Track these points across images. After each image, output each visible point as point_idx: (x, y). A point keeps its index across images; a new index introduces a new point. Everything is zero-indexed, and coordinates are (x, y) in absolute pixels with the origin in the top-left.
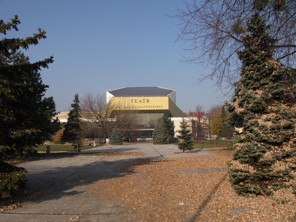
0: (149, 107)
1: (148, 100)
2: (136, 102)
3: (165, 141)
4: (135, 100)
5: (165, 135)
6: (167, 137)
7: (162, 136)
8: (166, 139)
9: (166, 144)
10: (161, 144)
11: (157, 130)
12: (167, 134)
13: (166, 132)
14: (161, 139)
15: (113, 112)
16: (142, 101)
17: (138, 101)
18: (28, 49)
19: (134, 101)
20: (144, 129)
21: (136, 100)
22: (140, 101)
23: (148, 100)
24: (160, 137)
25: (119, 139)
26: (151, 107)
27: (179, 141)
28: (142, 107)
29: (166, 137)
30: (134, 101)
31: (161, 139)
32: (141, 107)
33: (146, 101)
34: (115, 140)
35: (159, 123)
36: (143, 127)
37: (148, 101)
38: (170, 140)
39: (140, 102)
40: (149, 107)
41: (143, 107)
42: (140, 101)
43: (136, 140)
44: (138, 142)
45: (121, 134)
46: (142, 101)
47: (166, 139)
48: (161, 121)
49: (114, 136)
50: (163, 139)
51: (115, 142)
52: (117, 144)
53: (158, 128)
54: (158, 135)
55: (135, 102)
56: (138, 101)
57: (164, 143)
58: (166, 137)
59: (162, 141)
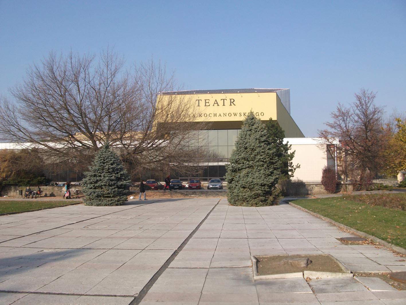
0: (235, 115)
1: (232, 101)
2: (207, 104)
3: (269, 193)
4: (205, 100)
5: (268, 172)
6: (276, 180)
7: (257, 174)
8: (273, 185)
9: (273, 204)
10: (256, 205)
11: (243, 155)
12: (275, 169)
13: (273, 163)
14: (257, 187)
15: (161, 126)
16: (221, 103)
17: (212, 102)
18: (342, 240)
19: (202, 103)
20: (215, 164)
21: (207, 101)
22: (216, 102)
23: (232, 101)
24: (250, 179)
25: (110, 185)
26: (238, 115)
27: (309, 192)
28: (220, 115)
29: (272, 179)
30: (202, 103)
31: (257, 187)
32: (218, 115)
33: (227, 103)
34: (97, 190)
35: (249, 133)
36: (216, 158)
37: (232, 102)
38: (283, 190)
39: (216, 105)
40: (235, 115)
41: (222, 115)
42: (216, 102)
43: (199, 188)
44: (202, 193)
45: (121, 169)
46: (221, 103)
47: (273, 185)
48: (255, 126)
49: (95, 176)
50: (263, 185)
51: (98, 196)
52: (105, 202)
53: (246, 148)
54: (244, 172)
55: (206, 106)
56: (212, 102)
57: (265, 203)
58: (272, 180)
59: (257, 195)
